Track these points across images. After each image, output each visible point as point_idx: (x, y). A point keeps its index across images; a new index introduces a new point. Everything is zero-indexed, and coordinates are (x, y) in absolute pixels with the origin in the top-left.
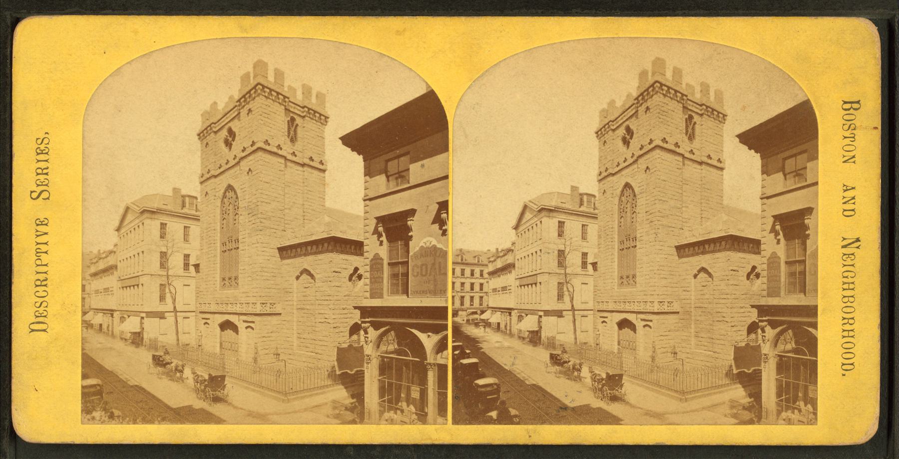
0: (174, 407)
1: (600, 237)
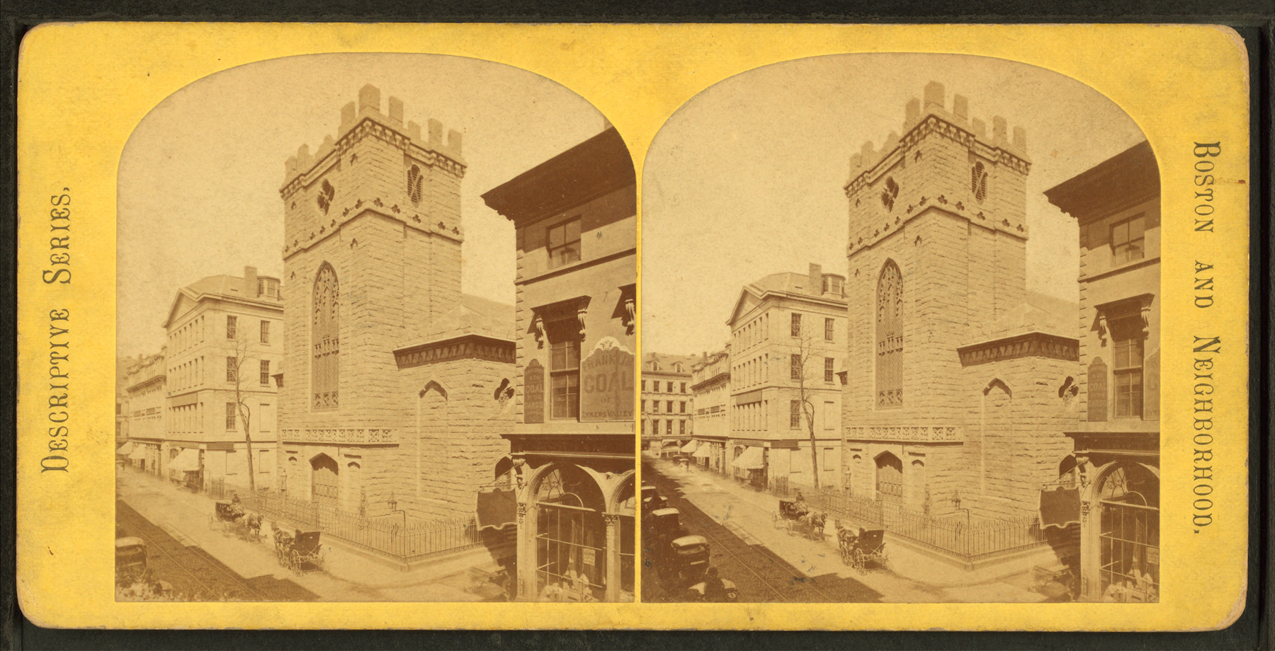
0: (247, 577)
1: (850, 336)
